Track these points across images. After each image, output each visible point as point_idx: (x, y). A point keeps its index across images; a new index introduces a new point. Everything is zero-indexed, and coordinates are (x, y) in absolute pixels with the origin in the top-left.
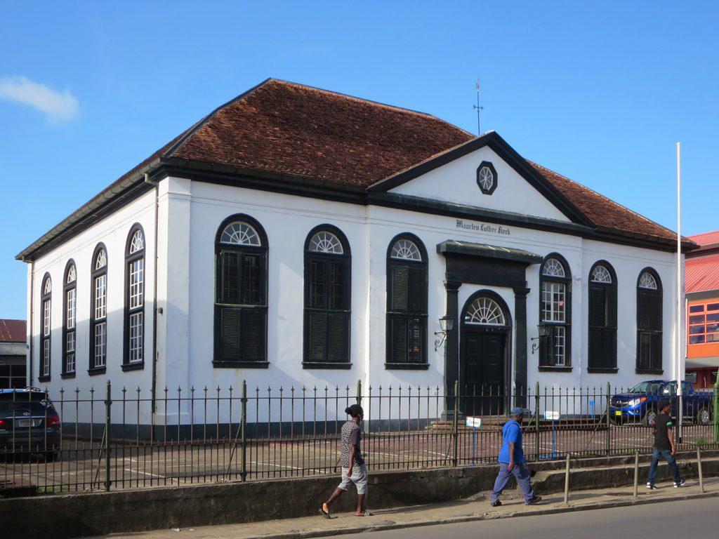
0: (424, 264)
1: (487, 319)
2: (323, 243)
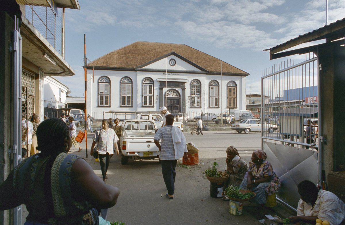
1: (172, 95)
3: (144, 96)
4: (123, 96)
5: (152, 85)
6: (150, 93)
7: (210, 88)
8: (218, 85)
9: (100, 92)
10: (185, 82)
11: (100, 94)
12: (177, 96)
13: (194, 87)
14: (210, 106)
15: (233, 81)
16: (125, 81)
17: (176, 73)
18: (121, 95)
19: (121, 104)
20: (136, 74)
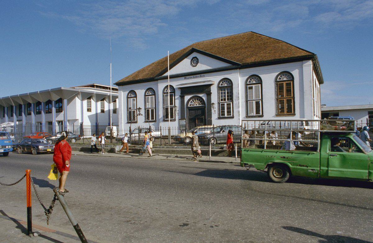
1: (196, 104)
2: (283, 78)
3: (166, 108)
4: (222, 104)
5: (260, 85)
6: (171, 103)
7: (248, 88)
8: (260, 81)
9: (129, 107)
10: (211, 85)
11: (129, 109)
13: (225, 90)
14: (249, 115)
15: (147, 89)
17: (199, 75)
18: (219, 103)
19: (145, 119)
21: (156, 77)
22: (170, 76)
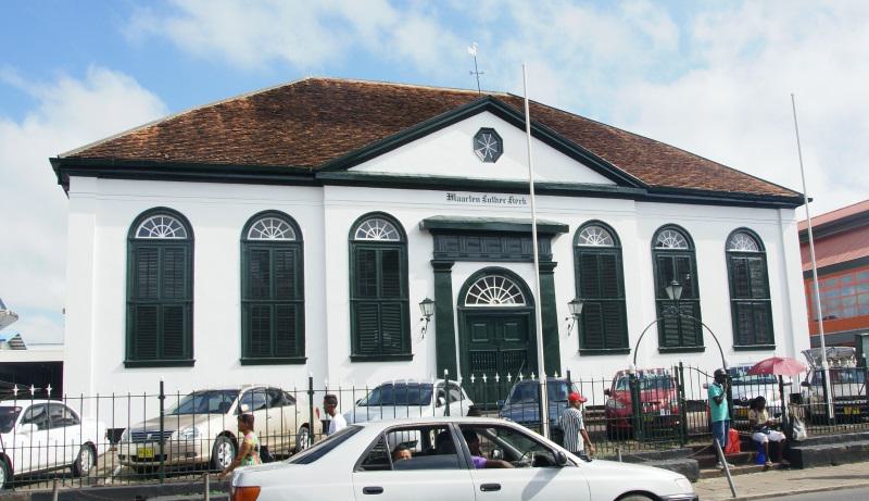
0: (404, 242)
1: (499, 300)
2: (266, 232)
12: (518, 300)
16: (151, 231)
20: (323, 192)
21: (325, 169)
22: (535, 184)
